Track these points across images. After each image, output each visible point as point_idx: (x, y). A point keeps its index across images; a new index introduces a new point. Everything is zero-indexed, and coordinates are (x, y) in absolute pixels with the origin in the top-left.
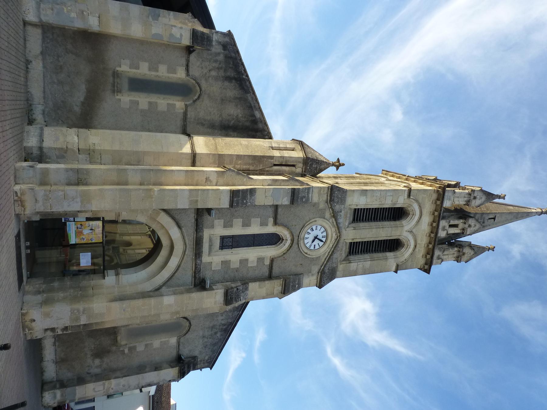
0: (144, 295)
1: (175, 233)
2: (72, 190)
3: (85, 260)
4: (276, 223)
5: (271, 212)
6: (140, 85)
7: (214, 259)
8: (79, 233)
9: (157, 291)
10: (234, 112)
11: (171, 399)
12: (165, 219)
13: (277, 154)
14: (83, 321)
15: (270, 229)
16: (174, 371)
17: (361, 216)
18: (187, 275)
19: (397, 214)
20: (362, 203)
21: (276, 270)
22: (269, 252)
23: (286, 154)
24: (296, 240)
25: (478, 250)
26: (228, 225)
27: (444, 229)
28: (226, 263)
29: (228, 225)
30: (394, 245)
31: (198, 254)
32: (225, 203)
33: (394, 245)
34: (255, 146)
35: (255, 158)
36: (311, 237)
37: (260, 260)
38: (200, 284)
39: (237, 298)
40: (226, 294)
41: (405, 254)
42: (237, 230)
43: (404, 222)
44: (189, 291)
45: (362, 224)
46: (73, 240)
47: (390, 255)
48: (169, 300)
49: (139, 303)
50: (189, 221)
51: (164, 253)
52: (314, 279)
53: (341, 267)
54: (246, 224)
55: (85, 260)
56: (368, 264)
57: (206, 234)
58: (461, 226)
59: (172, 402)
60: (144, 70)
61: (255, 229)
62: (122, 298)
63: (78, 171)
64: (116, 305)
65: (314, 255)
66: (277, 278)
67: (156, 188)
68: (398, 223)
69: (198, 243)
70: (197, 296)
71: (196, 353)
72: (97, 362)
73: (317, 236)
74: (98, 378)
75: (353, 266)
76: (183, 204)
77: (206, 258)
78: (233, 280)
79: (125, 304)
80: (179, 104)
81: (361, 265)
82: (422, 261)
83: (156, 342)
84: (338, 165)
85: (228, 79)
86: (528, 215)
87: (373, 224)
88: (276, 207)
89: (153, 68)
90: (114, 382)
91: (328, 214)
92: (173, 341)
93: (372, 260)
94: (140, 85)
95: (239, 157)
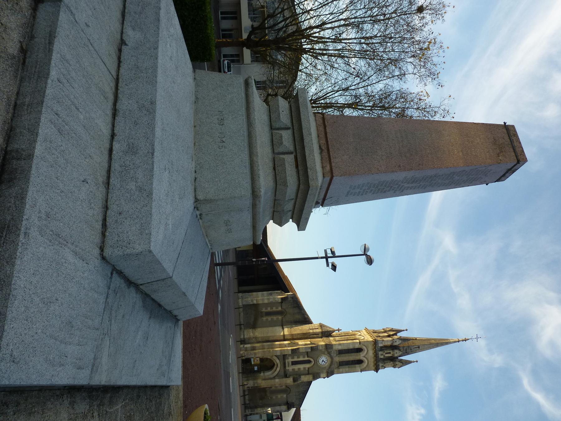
0: (271, 379)
1: (278, 361)
2: (252, 352)
3: (256, 368)
4: (308, 357)
5: (306, 354)
6: (268, 314)
7: (290, 368)
8: (254, 361)
9: (274, 378)
10: (298, 317)
12: (275, 358)
13: (311, 331)
14: (256, 385)
15: (306, 359)
16: (284, 407)
17: (341, 352)
19: (359, 350)
20: (340, 348)
21: (310, 372)
22: (307, 366)
23: (315, 331)
24: (316, 362)
27: (382, 355)
28: (293, 370)
30: (360, 362)
31: (285, 367)
32: (290, 353)
33: (360, 362)
34: (305, 328)
35: (303, 334)
37: (304, 368)
38: (286, 376)
39: (297, 381)
40: (293, 379)
41: (365, 365)
42: (296, 359)
43: (361, 353)
44: (283, 378)
47: (357, 366)
48: (277, 380)
49: (269, 381)
50: (282, 358)
51: (275, 366)
52: (325, 375)
53: (336, 370)
54: (298, 357)
55: (256, 368)
56: (347, 369)
57: (287, 361)
58: (392, 353)
60: (269, 309)
61: (301, 359)
62: (265, 379)
63: (253, 347)
64: (263, 381)
65: (323, 366)
67: (271, 350)
68: (358, 354)
69: (285, 364)
70: (285, 379)
71: (294, 401)
72: (261, 401)
73: (323, 360)
75: (341, 370)
76: (278, 354)
77: (287, 368)
78: (297, 375)
79: (266, 381)
80: (280, 317)
81: (344, 370)
82: (374, 368)
83: (279, 396)
84: (339, 330)
85: (294, 307)
86: (450, 343)
87: (346, 355)
88: (307, 352)
89: (272, 308)
91: (326, 353)
92: (285, 396)
93: (349, 368)
94: (268, 314)
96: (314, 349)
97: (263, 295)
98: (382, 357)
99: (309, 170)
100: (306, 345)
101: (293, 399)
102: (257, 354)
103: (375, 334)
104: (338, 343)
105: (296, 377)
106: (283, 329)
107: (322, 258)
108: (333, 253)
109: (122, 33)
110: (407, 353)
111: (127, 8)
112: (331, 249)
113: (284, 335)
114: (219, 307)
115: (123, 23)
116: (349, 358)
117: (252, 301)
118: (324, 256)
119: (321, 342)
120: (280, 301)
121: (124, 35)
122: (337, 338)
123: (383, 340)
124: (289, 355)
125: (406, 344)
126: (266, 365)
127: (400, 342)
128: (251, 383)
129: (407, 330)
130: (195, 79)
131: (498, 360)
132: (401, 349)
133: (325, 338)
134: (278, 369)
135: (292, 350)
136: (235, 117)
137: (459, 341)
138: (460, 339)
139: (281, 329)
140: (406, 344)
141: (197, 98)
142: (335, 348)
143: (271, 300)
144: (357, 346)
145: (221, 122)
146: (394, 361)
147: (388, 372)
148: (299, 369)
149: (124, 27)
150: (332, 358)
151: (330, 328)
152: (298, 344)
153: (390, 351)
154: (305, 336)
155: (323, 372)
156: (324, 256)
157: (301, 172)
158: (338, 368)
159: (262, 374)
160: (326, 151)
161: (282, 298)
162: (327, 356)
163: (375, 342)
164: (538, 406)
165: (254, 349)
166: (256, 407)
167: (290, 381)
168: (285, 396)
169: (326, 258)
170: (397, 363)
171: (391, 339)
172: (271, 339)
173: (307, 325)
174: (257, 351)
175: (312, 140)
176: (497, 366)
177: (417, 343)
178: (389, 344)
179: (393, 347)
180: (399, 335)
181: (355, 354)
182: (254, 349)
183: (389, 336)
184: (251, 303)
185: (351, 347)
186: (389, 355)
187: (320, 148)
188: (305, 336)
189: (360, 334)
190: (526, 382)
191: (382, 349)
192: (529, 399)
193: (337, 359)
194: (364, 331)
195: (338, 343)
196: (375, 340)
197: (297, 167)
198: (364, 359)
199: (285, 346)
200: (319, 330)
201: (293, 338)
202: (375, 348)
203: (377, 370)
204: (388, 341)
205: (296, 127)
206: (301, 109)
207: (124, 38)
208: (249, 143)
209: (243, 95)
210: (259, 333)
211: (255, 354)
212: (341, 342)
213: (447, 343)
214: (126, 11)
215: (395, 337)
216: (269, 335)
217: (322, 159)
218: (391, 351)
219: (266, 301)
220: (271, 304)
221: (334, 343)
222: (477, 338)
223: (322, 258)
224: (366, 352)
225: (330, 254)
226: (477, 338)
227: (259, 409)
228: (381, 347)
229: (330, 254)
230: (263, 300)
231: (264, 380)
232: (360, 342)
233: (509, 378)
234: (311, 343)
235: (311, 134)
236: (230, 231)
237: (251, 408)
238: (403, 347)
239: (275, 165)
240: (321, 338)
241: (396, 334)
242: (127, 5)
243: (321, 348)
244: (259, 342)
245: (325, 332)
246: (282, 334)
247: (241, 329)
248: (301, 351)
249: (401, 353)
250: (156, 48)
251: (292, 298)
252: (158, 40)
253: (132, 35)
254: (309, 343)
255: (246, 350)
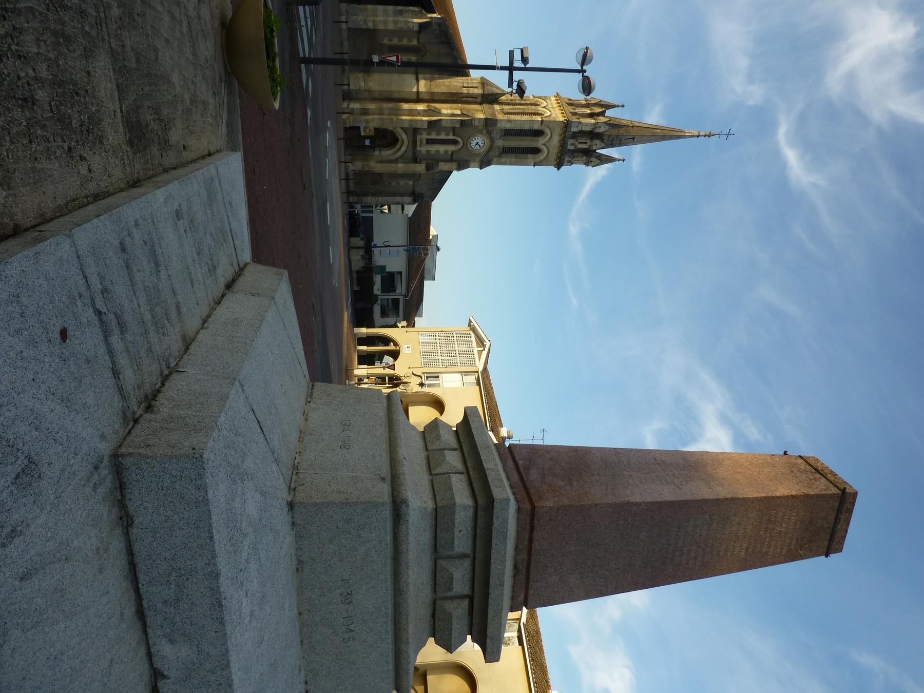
0: (390, 162)
1: (404, 136)
4: (454, 135)
8: (365, 131)
9: (396, 161)
11: (431, 227)
13: (465, 91)
15: (451, 137)
17: (508, 133)
18: (410, 155)
19: (539, 133)
20: (508, 126)
21: (455, 157)
22: (451, 148)
23: (472, 91)
24: (466, 144)
25: (610, 160)
26: (429, 134)
27: (573, 144)
29: (429, 134)
30: (536, 151)
31: (415, 145)
32: (426, 126)
33: (536, 151)
36: (475, 143)
37: (446, 152)
38: (415, 160)
39: (433, 169)
41: (542, 156)
42: (434, 136)
43: (540, 138)
44: (410, 162)
45: (509, 138)
46: (363, 134)
47: (530, 156)
48: (400, 165)
51: (400, 144)
52: (477, 164)
53: (495, 160)
54: (438, 134)
55: (367, 142)
56: (513, 160)
57: (419, 137)
59: (433, 232)
60: (395, 41)
62: (381, 162)
64: (378, 164)
65: (477, 152)
66: (455, 161)
67: (394, 118)
68: (535, 138)
69: (415, 141)
73: (478, 142)
74: (373, 195)
75: (503, 160)
76: (406, 126)
77: (418, 148)
81: (508, 160)
82: (555, 163)
83: (402, 182)
86: (685, 137)
87: (517, 138)
89: (400, 40)
90: (380, 198)
91: (484, 132)
92: (411, 183)
93: (516, 157)
95: (442, 93)
96: (465, 126)
97: (386, 12)
98: (572, 148)
99: (488, 640)
100: (453, 115)
101: (422, 188)
102: (371, 123)
103: (571, 109)
104: (506, 117)
105: (432, 162)
106: (417, 80)
107: (503, 68)
108: (525, 60)
109: (149, 655)
110: (611, 145)
111: (144, 596)
112: (522, 51)
113: (418, 92)
114: (309, 113)
115: (145, 633)
116: (519, 144)
117: (365, 22)
118: (507, 64)
119: (479, 113)
120: (416, 28)
121: (155, 659)
122: (507, 108)
123: (580, 123)
124: (425, 129)
125: (615, 132)
126: (385, 138)
127: (607, 128)
128: (358, 165)
129: (623, 106)
130: (293, 524)
131: (756, 94)
132: (606, 138)
133: (486, 106)
134: (404, 148)
135: (429, 122)
136: (373, 587)
137: (698, 136)
138: (702, 134)
139: (414, 81)
140: (615, 132)
141: (300, 562)
142: (500, 125)
143: (400, 25)
144: (536, 127)
145: (347, 598)
146: (590, 157)
147: (576, 170)
148: (437, 152)
149: (151, 643)
150: (492, 140)
151: (498, 88)
152: (439, 113)
153: (585, 139)
154: (453, 98)
155: (474, 160)
156: (507, 64)
157: (475, 621)
158: (500, 156)
159: (377, 153)
160: (524, 571)
161: (420, 25)
162: (484, 138)
163: (567, 124)
164: (784, 166)
165: (365, 112)
166: (365, 194)
167: (420, 168)
168: (411, 183)
169: (511, 69)
170: (593, 159)
171: (593, 121)
172: (396, 96)
173: (460, 79)
174: (370, 117)
175: (502, 594)
176: (751, 103)
177: (633, 132)
178: (588, 129)
179: (593, 135)
180: (609, 113)
181: (531, 138)
182: (365, 112)
183: (591, 115)
184: (364, 27)
185: (527, 127)
186: (584, 146)
187: (516, 567)
188: (453, 98)
189: (545, 104)
190: (782, 132)
191: (575, 136)
192: (776, 156)
193: (500, 143)
194: (553, 98)
195: (506, 117)
196: (568, 121)
197: (475, 527)
198: (544, 148)
199: (418, 113)
200: (478, 91)
201: (433, 98)
202: (564, 133)
203: (559, 166)
204: (587, 124)
205: (479, 556)
206: (494, 541)
207: (158, 665)
208: (395, 620)
209: (389, 538)
210: (378, 82)
211: (367, 121)
212: (513, 117)
213: (679, 137)
214: (145, 603)
215: (602, 119)
216: (394, 88)
217: (514, 586)
218: (588, 141)
219: (391, 26)
220: (400, 33)
221: (500, 117)
222: (728, 135)
223: (503, 68)
224: (548, 137)
225: (518, 63)
226: (728, 135)
227: (370, 198)
228: (575, 133)
229: (518, 63)
230: (385, 22)
231: (379, 162)
232: (542, 121)
233: (762, 120)
234: (463, 115)
235: (502, 585)
236: (345, 446)
237: (357, 195)
238: (609, 136)
239: (434, 610)
240: (481, 104)
241: (602, 114)
242: (143, 590)
243: (477, 124)
244: (374, 100)
245: (489, 95)
246: (415, 90)
247: (343, 70)
248: (444, 124)
249: (603, 145)
250: (227, 666)
251: (439, 25)
252: (227, 650)
253: (171, 655)
254: (459, 112)
255: (351, 112)
